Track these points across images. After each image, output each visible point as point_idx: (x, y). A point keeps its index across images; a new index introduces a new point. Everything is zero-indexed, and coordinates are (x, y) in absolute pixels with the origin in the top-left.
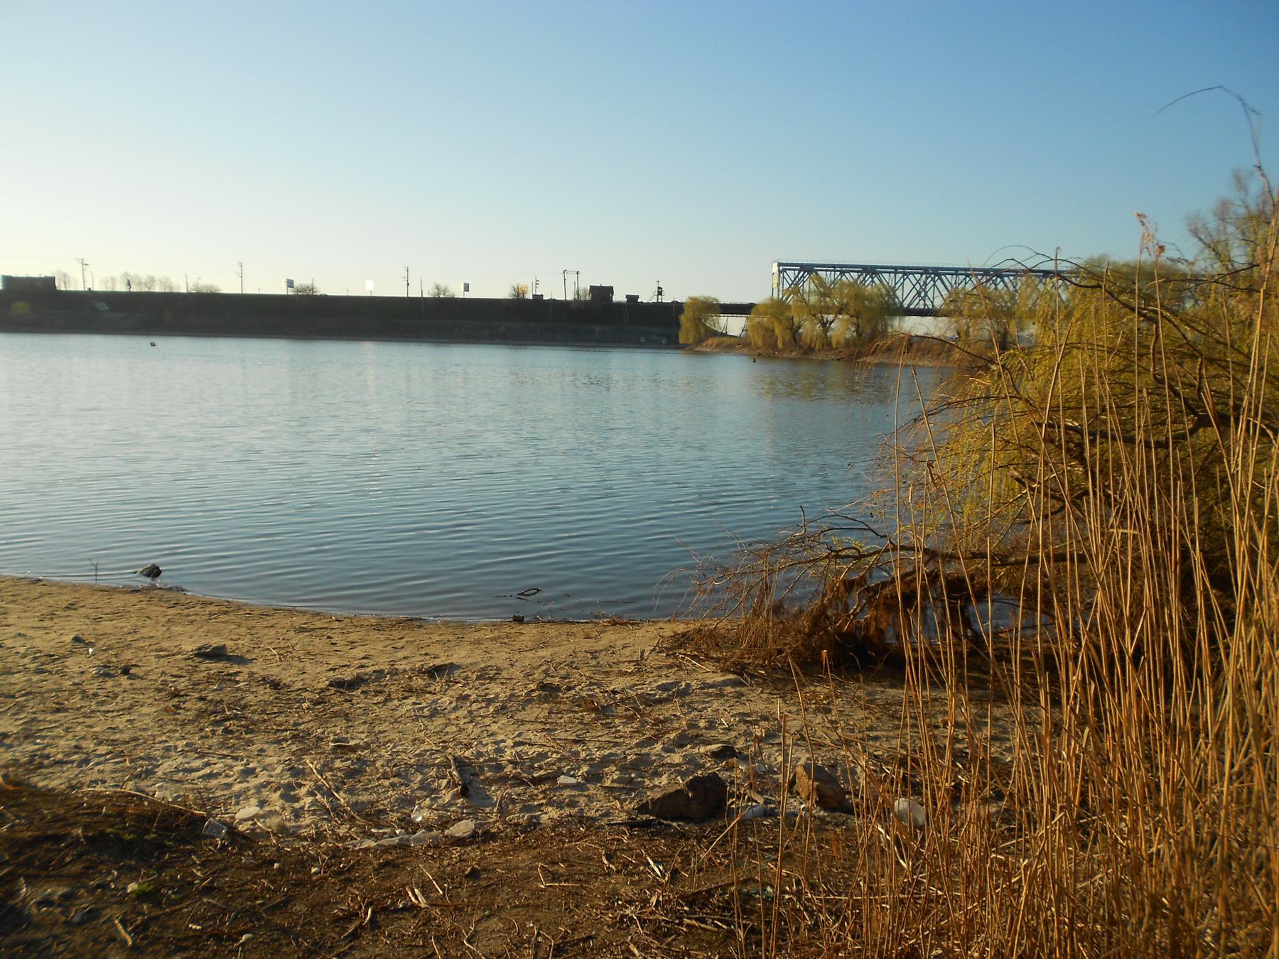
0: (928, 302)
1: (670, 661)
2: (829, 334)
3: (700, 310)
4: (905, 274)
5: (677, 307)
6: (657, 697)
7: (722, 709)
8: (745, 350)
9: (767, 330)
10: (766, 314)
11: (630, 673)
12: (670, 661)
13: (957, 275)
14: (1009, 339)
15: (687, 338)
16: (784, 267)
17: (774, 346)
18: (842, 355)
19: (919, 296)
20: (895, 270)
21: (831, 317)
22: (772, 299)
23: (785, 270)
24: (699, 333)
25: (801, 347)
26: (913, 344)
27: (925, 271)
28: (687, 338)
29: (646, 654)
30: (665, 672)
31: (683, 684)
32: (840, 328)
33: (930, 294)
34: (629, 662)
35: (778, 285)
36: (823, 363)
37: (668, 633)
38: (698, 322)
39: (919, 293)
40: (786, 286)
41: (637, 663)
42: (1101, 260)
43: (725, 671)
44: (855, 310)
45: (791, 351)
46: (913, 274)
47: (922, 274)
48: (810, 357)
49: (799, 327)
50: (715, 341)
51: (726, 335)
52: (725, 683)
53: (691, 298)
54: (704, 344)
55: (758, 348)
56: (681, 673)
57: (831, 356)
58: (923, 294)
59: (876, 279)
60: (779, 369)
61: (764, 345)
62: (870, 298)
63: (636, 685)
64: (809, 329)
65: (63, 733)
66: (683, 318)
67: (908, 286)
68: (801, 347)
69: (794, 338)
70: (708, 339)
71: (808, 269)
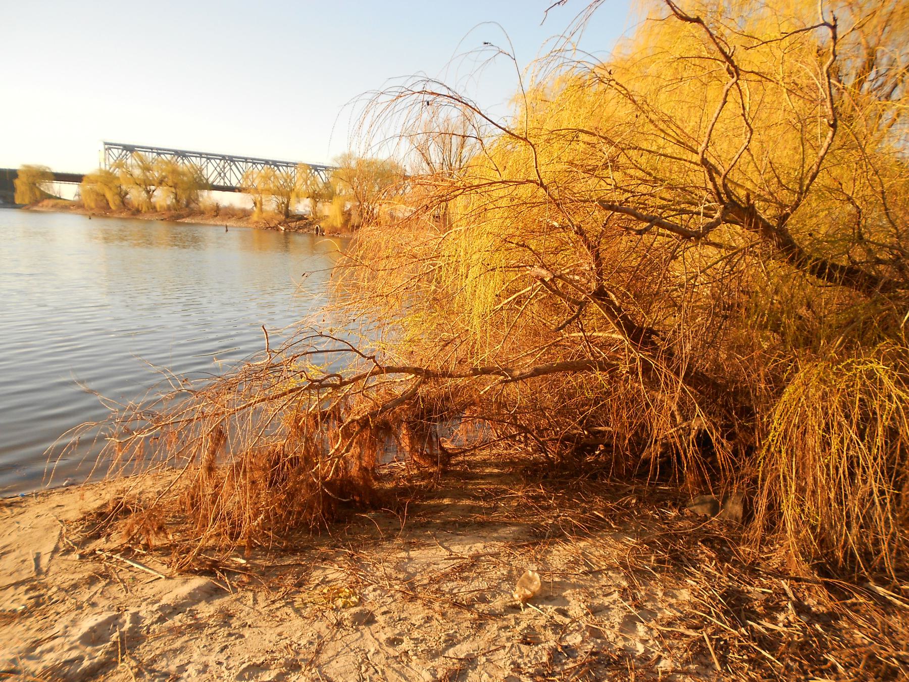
1: (89, 568)
2: (152, 200)
3: (34, 176)
4: (208, 159)
5: (13, 174)
6: (86, 663)
7: (212, 659)
8: (80, 211)
9: (98, 194)
10: (97, 182)
11: (23, 613)
12: (89, 568)
13: (247, 162)
15: (23, 200)
16: (109, 146)
17: (107, 207)
18: (165, 217)
20: (200, 155)
21: (153, 188)
22: (101, 170)
23: (110, 149)
24: (34, 194)
25: (129, 209)
26: (217, 211)
27: (223, 158)
28: (23, 200)
29: (44, 561)
30: (85, 595)
31: (127, 617)
32: (162, 197)
33: (228, 175)
34: (17, 585)
35: (105, 160)
36: (149, 221)
37: (73, 514)
38: (33, 186)
40: (112, 161)
41: (32, 585)
42: (348, 157)
43: (187, 571)
44: (173, 182)
45: (121, 212)
46: (214, 159)
47: (221, 160)
48: (138, 217)
49: (127, 194)
50: (51, 202)
51: (60, 198)
52: (194, 598)
53: (25, 166)
54: (40, 205)
55: (92, 209)
56: (114, 590)
57: (155, 217)
59: (186, 161)
60: (113, 225)
61: (97, 207)
62: (184, 174)
63: (38, 643)
64: (136, 196)
66: (17, 182)
68: (129, 209)
69: (123, 202)
70: (43, 200)
71: (130, 149)
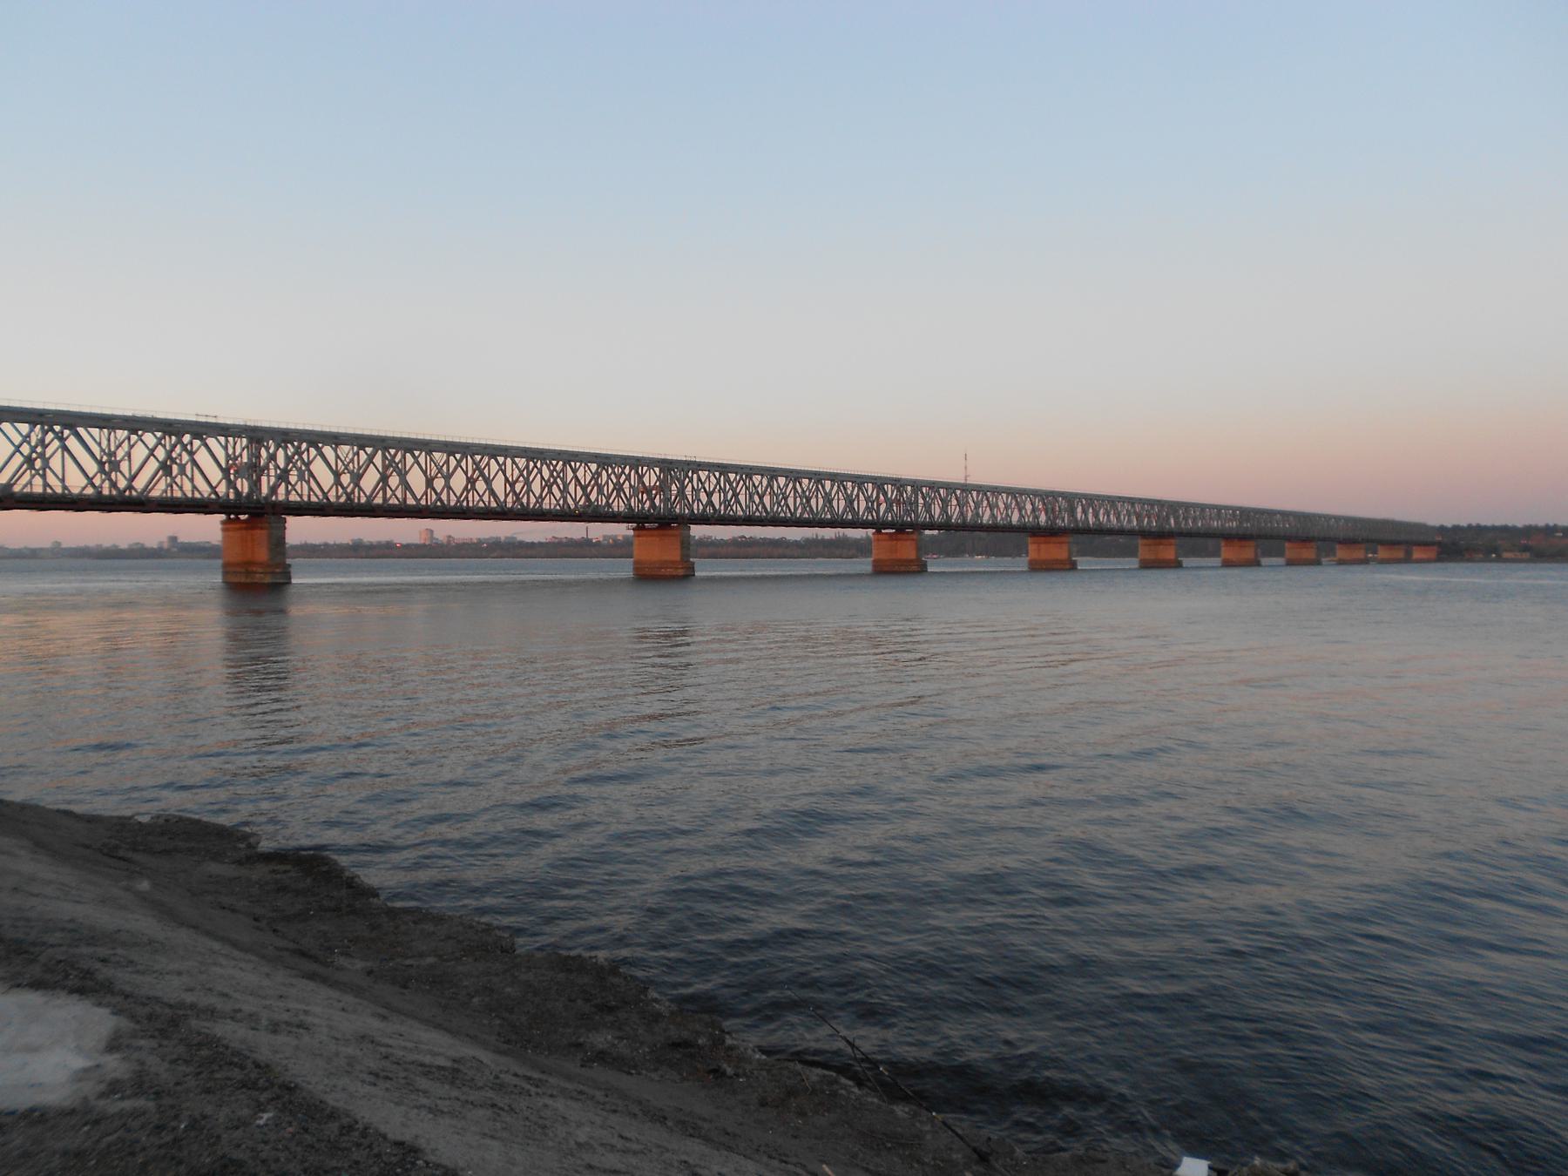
0: (51, 479)
14: (102, 1087)
19: (31, 466)
33: (55, 463)
39: (29, 461)
58: (38, 464)
65: (425, 673)
67: (140, 453)
